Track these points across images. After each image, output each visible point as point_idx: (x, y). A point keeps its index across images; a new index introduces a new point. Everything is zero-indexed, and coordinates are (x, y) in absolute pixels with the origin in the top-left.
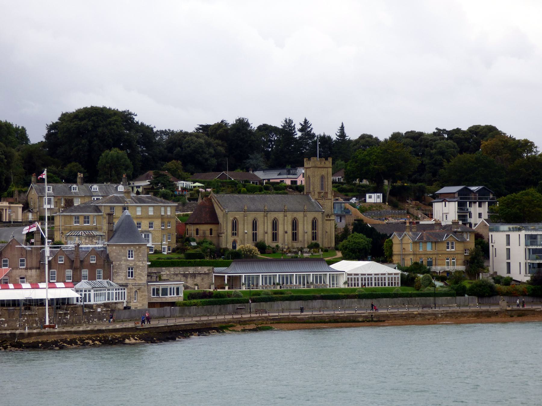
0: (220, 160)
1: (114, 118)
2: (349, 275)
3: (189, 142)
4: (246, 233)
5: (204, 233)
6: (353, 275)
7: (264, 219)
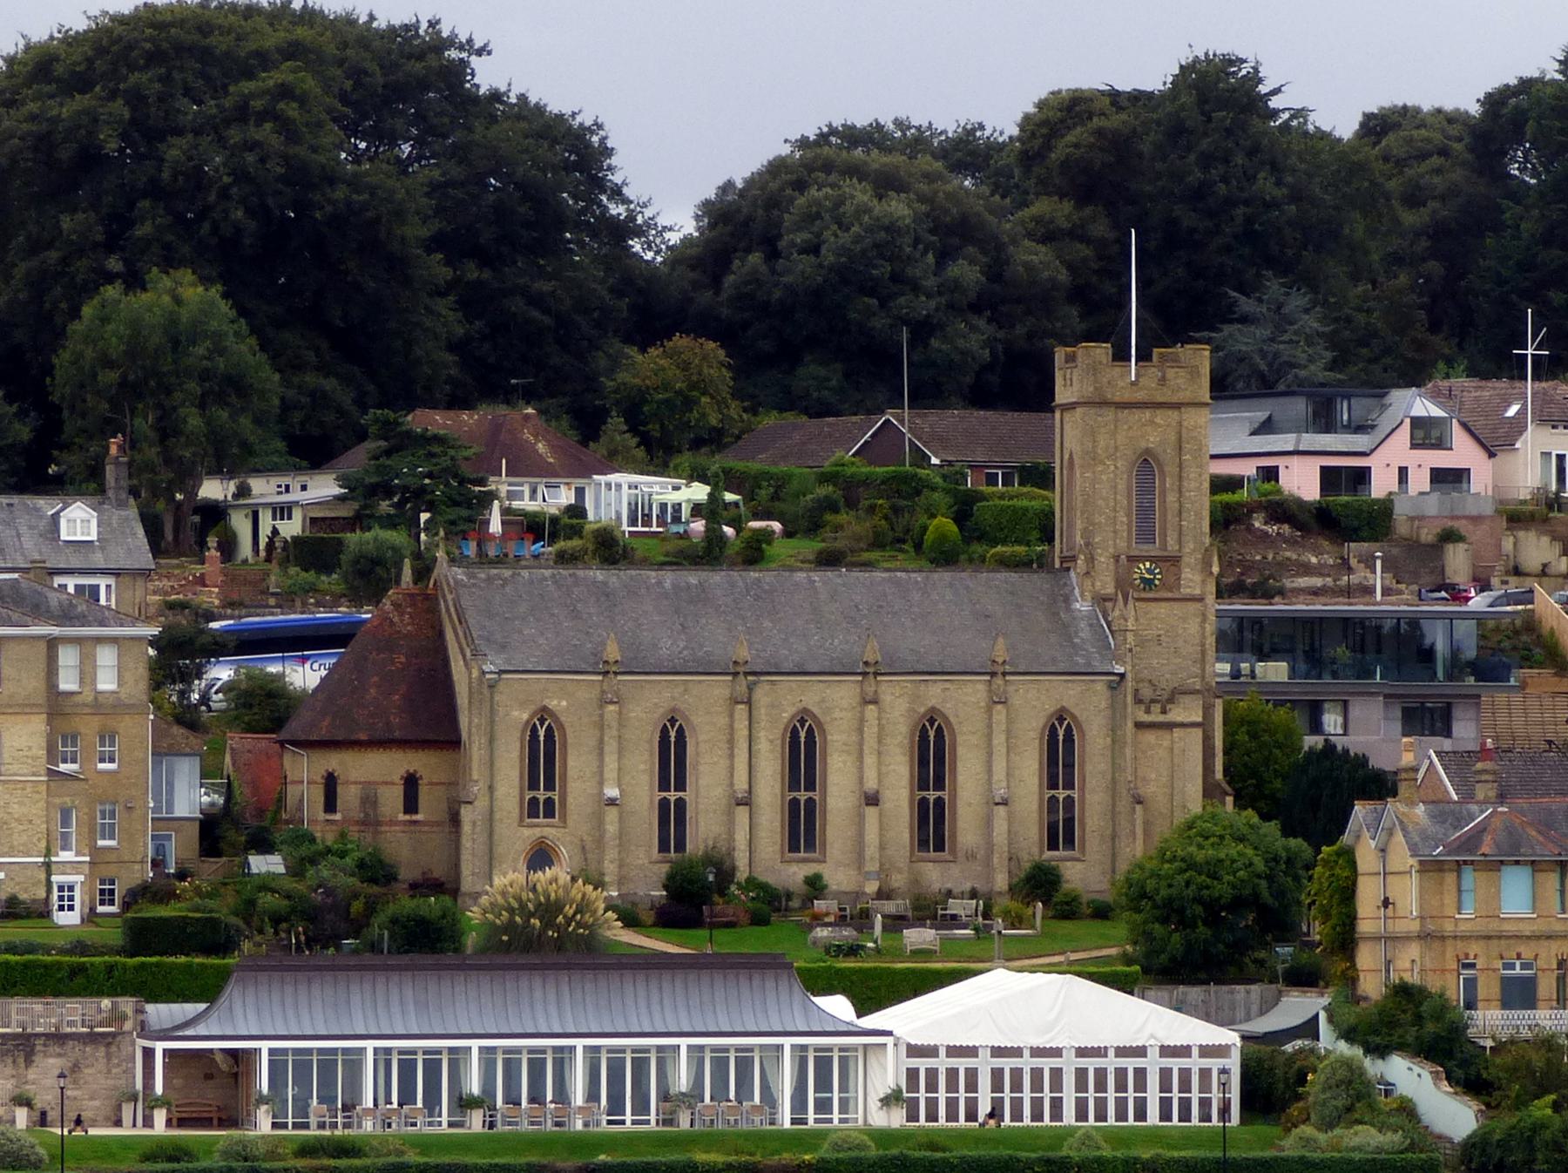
0: (1020, 330)
1: (282, 74)
2: (915, 1051)
3: (818, 216)
4: (612, 802)
5: (369, 800)
6: (942, 1052)
7: (731, 716)
